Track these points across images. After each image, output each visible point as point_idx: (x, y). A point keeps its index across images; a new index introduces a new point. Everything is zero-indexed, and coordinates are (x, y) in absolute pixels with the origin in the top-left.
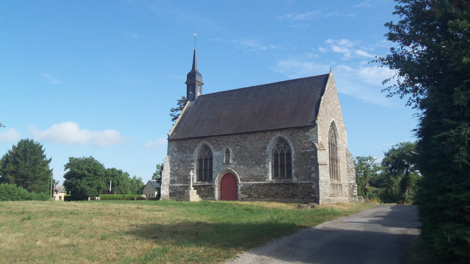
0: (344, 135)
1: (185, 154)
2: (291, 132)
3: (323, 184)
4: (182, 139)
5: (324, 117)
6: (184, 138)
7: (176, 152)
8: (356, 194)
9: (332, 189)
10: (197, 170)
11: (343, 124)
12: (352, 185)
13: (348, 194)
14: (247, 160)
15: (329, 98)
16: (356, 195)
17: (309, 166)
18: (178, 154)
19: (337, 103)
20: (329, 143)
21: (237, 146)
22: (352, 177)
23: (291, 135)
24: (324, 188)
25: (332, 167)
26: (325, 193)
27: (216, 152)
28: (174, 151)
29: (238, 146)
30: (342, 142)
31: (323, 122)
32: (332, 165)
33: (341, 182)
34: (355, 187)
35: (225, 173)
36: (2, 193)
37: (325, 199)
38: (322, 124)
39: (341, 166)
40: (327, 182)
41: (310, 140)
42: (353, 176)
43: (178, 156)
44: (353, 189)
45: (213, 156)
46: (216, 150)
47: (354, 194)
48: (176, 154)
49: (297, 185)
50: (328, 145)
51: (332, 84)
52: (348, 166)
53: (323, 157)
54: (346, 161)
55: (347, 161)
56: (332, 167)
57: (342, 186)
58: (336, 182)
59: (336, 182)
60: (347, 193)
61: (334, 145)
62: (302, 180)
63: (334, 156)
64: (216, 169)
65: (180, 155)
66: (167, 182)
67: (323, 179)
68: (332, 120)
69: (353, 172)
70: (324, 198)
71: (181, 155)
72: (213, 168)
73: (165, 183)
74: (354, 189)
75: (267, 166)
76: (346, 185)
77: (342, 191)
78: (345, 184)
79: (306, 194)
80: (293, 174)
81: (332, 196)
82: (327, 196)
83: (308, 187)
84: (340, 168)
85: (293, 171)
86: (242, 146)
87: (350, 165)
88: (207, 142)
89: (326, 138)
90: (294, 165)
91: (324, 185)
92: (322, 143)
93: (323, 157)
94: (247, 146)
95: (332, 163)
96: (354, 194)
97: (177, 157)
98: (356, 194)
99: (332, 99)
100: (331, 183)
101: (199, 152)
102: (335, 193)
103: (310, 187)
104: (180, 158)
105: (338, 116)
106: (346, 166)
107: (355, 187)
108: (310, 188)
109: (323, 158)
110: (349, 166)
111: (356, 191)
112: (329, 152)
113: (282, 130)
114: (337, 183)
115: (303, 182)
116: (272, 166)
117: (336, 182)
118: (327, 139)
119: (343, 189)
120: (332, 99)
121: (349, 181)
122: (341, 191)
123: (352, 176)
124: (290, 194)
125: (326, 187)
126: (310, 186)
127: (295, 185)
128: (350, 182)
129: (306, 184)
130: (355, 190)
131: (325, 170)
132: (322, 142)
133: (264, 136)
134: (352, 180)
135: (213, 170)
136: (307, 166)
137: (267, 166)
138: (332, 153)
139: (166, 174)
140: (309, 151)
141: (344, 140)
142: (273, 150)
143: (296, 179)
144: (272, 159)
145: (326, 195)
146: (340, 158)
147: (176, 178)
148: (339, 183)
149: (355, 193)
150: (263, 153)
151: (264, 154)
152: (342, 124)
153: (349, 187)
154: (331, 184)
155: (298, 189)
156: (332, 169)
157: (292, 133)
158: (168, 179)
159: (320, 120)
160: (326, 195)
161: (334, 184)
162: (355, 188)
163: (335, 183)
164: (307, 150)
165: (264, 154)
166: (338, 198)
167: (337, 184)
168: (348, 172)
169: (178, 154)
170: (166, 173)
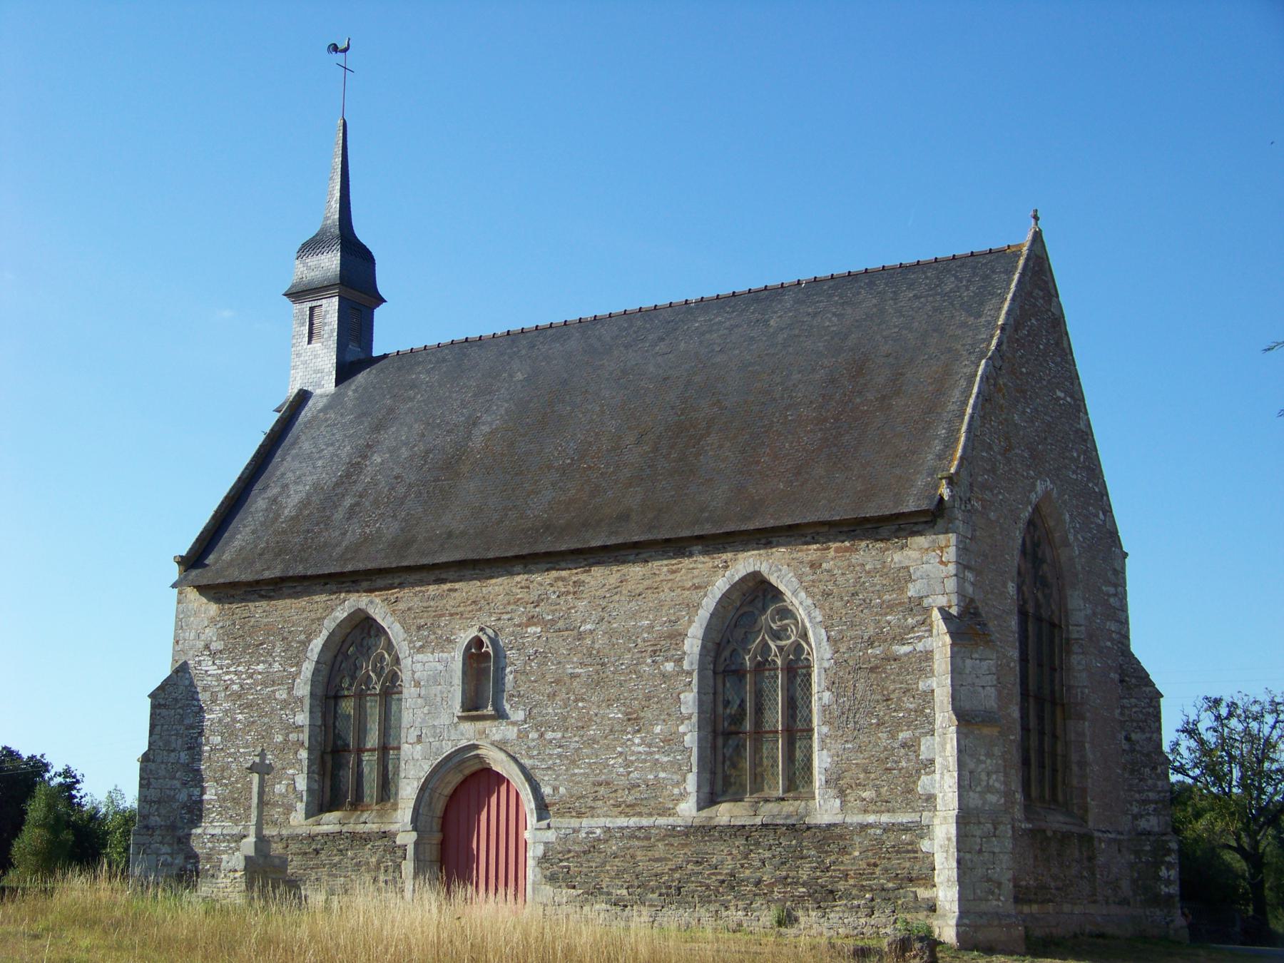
0: (1109, 573)
1: (261, 667)
2: (818, 549)
3: (978, 833)
4: (249, 584)
5: (993, 471)
6: (258, 582)
7: (213, 655)
8: (1172, 891)
9: (1036, 857)
10: (323, 753)
11: (1101, 516)
12: (1152, 838)
13: (1126, 887)
14: (583, 700)
15: (1022, 373)
16: (1170, 896)
17: (903, 735)
18: (229, 666)
19: (1068, 399)
20: (1023, 614)
21: (531, 621)
22: (1152, 795)
23: (814, 566)
24: (980, 851)
25: (1041, 743)
26: (989, 880)
27: (420, 657)
28: (207, 647)
29: (535, 624)
30: (1099, 609)
31: (988, 496)
32: (1042, 733)
33: (1091, 824)
34: (1168, 852)
35: (467, 772)
36: (753, 961)
37: (985, 913)
38: (977, 505)
39: (1088, 739)
40: (998, 824)
41: (912, 591)
42: (1159, 792)
43: (228, 673)
44: (1157, 865)
45: (405, 676)
46: (421, 647)
47: (1163, 887)
48: (214, 664)
49: (841, 837)
50: (1013, 623)
51: (1043, 298)
52: (1128, 739)
53: (983, 687)
54: (1122, 714)
55: (1127, 712)
56: (1041, 743)
57: (1096, 843)
58: (1056, 822)
59: (1058, 822)
60: (1125, 884)
61: (1053, 625)
62: (866, 811)
63: (1052, 681)
64: (419, 747)
65: (236, 673)
66: (163, 812)
67: (980, 802)
68: (1038, 488)
69: (1154, 768)
70: (984, 907)
71: (240, 668)
72: (403, 740)
73: (157, 818)
74: (1163, 862)
75: (685, 734)
76: (1115, 840)
77: (1093, 874)
78: (1112, 836)
79: (890, 885)
80: (818, 778)
81: (1032, 897)
82: (998, 900)
83: (898, 850)
84: (1087, 745)
85: (821, 761)
86: (553, 622)
87: (1143, 731)
88: (378, 600)
89: (1005, 585)
90: (825, 729)
91: (981, 838)
92: (976, 608)
93: (983, 687)
94: (584, 621)
95: (1041, 719)
96: (1164, 890)
97: (218, 678)
98: (1174, 889)
99: (1041, 379)
100: (1031, 826)
101: (336, 657)
102: (1053, 884)
103: (910, 847)
104: (236, 687)
105: (1074, 472)
106: (1122, 735)
107: (1168, 852)
108: (908, 852)
109: (980, 689)
110: (1133, 736)
111: (1173, 874)
112: (1024, 659)
113: (764, 538)
114: (1065, 828)
115: (871, 818)
116: (326, 646)
117: (1056, 822)
118: (1011, 588)
119: (1101, 859)
120: (1041, 379)
121: (1136, 817)
122: (1085, 874)
123: (1150, 794)
124: (804, 885)
125: (997, 850)
126: (911, 843)
127: (830, 836)
128: (1143, 824)
129: (887, 829)
130: (1169, 866)
131: (989, 755)
132: (978, 604)
133: (674, 572)
134: (1148, 814)
135: (402, 753)
136: (893, 737)
137: (685, 734)
138: (1040, 665)
139: (162, 773)
140: (906, 649)
141: (1112, 600)
142: (719, 644)
143: (838, 801)
144: (715, 694)
145: (993, 893)
146: (1082, 693)
147: (213, 791)
148: (1075, 829)
149: (1168, 882)
150: (667, 660)
151: (669, 666)
152: (1097, 516)
153: (1137, 853)
154: (1030, 830)
155: (846, 859)
156: (1041, 751)
157: (819, 553)
158: (168, 796)
159: (971, 485)
160: (993, 893)
161: (1049, 834)
162: (1167, 859)
163: (1056, 826)
164: (895, 648)
165: (669, 666)
166: (1066, 908)
167: (1065, 838)
168: (1132, 772)
169: (229, 666)
170: (163, 766)
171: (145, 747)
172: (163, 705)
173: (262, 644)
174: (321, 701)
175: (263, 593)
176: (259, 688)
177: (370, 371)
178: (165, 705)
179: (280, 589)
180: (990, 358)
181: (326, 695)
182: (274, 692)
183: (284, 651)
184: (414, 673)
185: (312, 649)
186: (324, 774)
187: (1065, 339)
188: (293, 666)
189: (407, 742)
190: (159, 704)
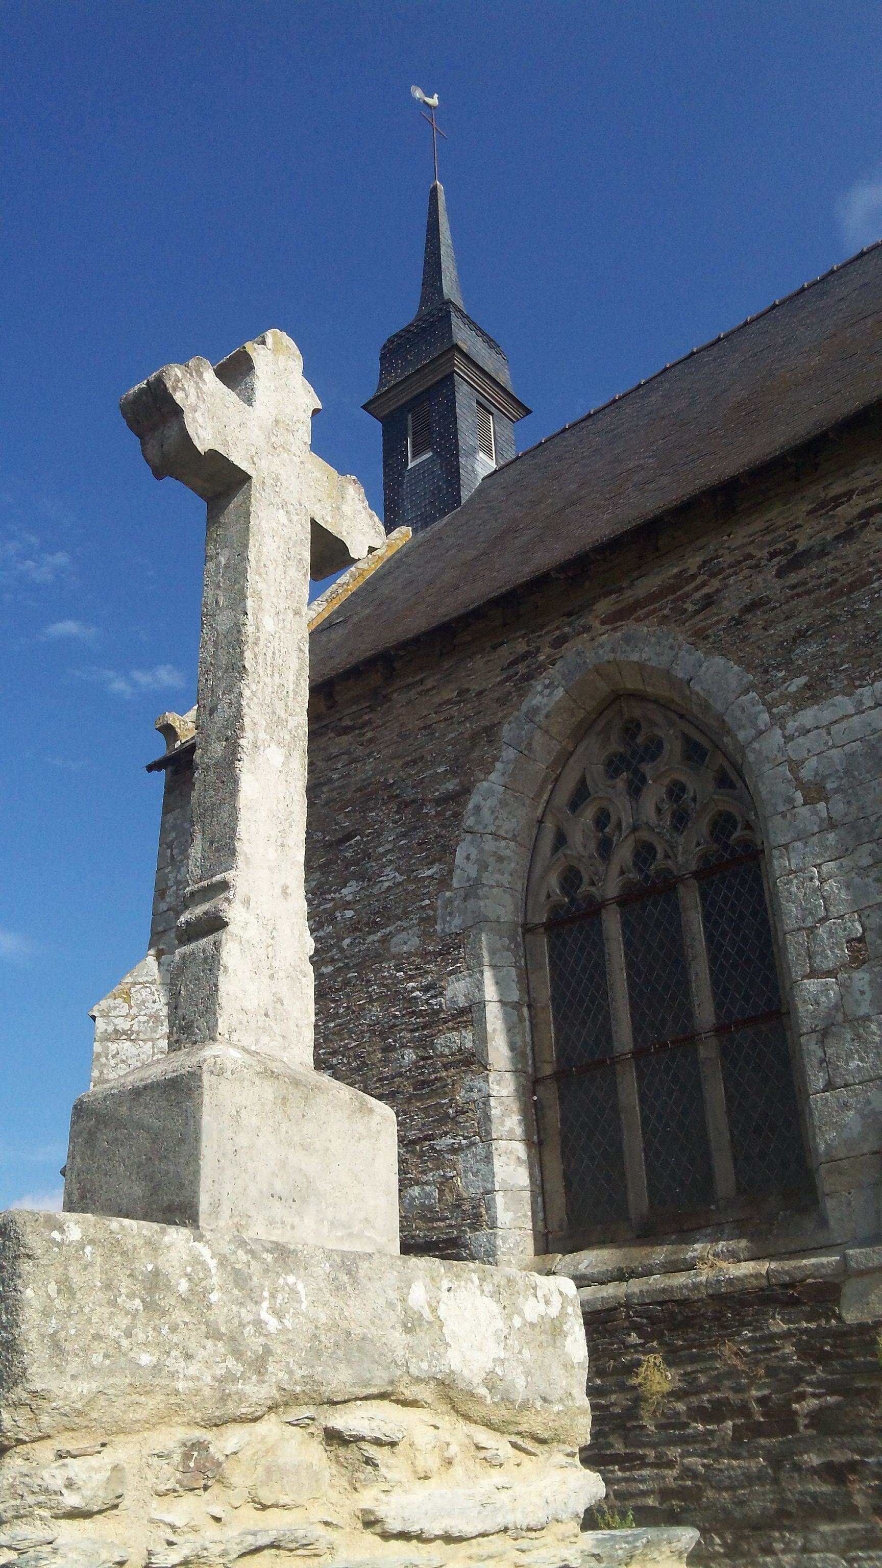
171: (310, 945)
172: (124, 1033)
173: (349, 837)
174: (512, 939)
175: (347, 722)
176: (347, 941)
177: (255, 499)
178: (129, 1035)
179: (387, 698)
180: (640, 1053)
181: (524, 925)
182: (385, 940)
183: (404, 835)
184: (795, 766)
185: (478, 809)
186: (541, 1143)
187: (554, 1224)
188: (432, 863)
189: (813, 974)
190: (116, 1031)
